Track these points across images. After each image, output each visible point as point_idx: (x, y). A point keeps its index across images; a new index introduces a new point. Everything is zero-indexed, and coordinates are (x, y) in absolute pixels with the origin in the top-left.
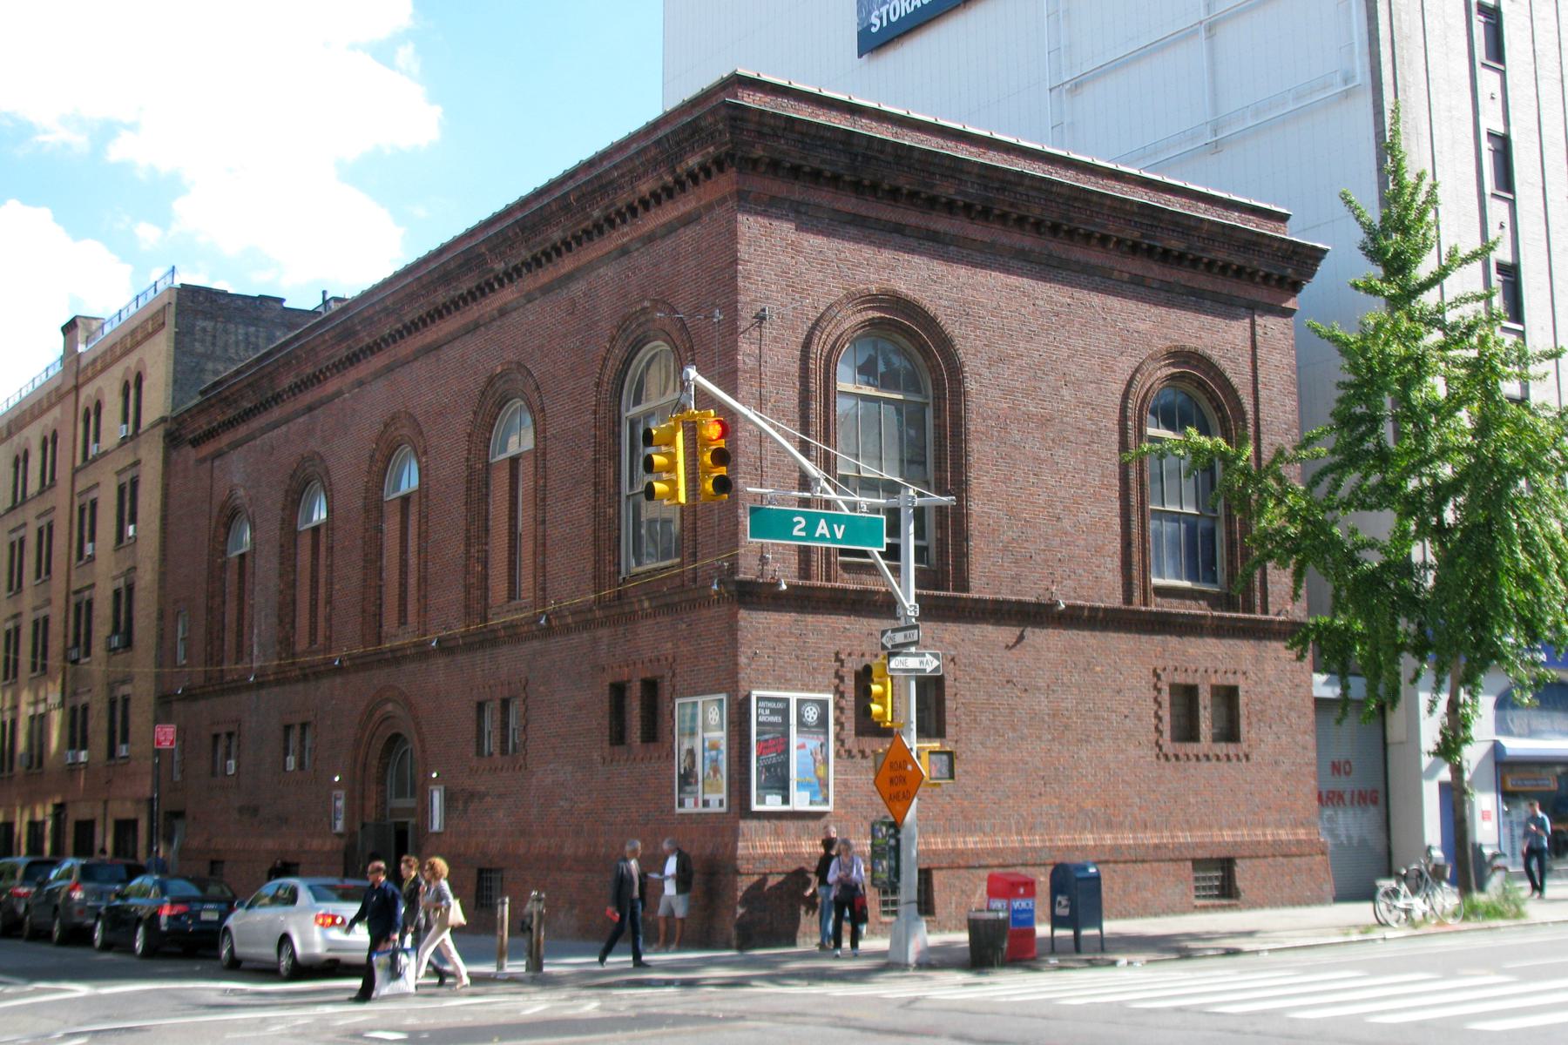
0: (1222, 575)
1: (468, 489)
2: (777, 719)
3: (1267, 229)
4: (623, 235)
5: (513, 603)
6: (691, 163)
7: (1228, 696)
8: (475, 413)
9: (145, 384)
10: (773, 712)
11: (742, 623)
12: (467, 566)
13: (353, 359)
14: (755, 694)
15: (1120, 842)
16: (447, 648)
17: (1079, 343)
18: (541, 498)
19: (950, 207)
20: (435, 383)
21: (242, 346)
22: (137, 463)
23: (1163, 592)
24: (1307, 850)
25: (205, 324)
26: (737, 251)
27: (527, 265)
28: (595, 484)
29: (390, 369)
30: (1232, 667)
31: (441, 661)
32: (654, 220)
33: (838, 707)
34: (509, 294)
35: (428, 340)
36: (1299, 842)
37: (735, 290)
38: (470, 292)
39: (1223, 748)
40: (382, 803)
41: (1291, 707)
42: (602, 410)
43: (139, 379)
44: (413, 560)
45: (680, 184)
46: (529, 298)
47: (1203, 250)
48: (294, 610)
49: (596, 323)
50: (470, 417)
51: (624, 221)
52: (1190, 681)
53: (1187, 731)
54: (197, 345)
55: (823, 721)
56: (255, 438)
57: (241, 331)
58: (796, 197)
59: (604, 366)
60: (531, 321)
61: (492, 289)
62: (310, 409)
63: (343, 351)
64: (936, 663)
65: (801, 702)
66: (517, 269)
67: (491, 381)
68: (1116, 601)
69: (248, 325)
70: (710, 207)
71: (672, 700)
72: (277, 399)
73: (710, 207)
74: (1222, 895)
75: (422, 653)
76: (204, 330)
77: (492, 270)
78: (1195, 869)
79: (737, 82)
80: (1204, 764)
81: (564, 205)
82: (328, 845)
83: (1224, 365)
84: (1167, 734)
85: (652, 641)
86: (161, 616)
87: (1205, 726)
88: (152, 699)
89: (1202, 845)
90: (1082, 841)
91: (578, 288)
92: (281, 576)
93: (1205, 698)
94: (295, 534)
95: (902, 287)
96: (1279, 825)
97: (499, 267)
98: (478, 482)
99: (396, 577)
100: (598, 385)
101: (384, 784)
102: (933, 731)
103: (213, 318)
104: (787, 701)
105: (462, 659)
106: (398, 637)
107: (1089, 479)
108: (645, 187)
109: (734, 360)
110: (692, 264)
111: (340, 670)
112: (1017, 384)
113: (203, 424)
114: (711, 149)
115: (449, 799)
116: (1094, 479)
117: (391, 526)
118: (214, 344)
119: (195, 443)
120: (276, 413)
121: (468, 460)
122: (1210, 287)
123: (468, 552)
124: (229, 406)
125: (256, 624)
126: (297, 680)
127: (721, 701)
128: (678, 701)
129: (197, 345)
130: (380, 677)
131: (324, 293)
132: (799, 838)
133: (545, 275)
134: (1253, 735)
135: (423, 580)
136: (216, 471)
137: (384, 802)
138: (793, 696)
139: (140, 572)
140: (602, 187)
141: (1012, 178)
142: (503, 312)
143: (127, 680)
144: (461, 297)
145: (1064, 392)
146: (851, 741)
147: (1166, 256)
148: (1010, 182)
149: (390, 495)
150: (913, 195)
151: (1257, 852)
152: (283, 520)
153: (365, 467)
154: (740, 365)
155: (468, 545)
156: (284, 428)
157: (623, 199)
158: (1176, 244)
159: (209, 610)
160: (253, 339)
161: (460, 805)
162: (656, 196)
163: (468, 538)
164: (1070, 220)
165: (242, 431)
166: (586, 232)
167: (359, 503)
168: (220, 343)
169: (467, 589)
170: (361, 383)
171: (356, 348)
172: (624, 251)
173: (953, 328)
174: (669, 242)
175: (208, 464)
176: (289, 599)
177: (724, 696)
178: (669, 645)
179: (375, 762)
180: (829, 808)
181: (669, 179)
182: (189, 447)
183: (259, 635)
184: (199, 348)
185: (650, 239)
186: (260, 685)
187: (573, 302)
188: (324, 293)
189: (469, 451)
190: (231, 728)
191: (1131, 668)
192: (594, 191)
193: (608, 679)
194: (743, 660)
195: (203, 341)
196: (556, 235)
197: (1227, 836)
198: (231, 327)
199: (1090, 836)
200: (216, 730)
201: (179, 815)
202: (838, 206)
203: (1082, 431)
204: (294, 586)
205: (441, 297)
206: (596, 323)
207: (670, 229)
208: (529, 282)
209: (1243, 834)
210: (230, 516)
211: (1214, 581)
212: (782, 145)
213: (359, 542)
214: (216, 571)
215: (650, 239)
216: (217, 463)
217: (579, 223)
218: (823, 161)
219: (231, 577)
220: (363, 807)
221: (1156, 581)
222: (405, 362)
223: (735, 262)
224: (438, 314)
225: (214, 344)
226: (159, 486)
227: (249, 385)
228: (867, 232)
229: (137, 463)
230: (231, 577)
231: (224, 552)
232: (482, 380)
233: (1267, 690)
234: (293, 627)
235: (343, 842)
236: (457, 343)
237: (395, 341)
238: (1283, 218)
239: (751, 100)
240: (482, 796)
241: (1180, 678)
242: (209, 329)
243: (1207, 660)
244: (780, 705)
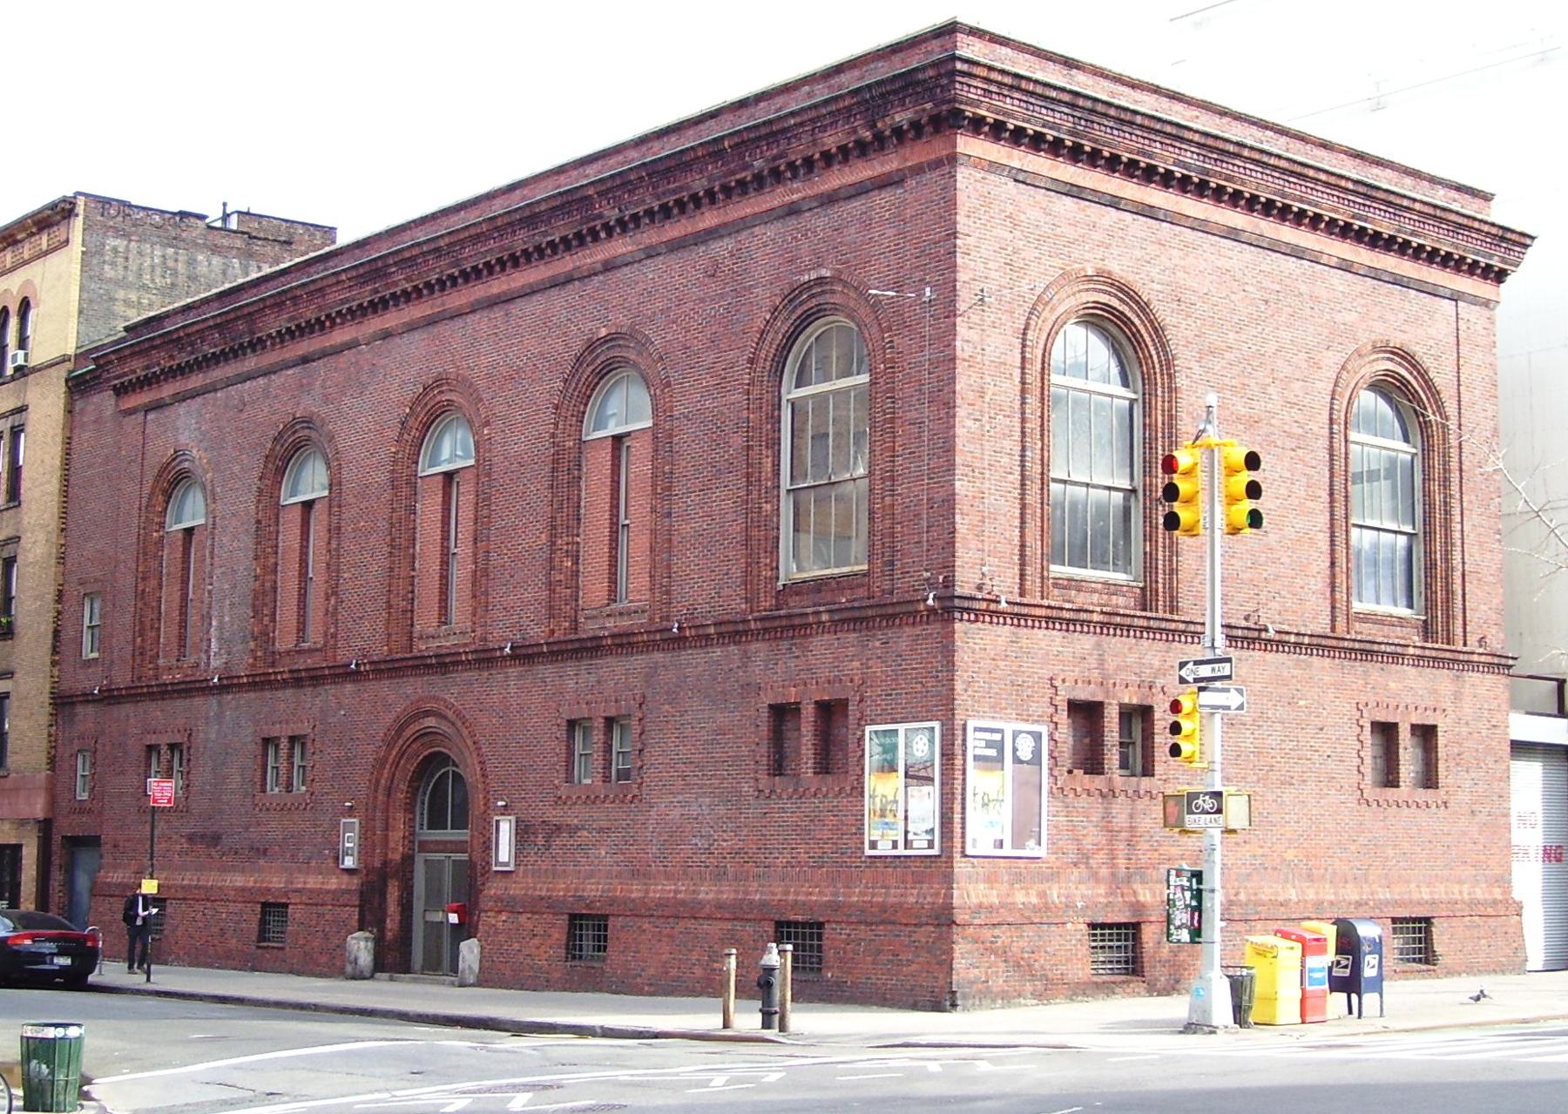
2: (992, 752)
3: (1470, 207)
4: (794, 192)
5: (613, 606)
6: (897, 118)
10: (989, 744)
11: (958, 643)
13: (378, 306)
14: (971, 724)
15: (1321, 896)
16: (525, 655)
17: (1285, 335)
18: (663, 486)
20: (510, 342)
21: (158, 271)
22: (22, 410)
23: (1365, 618)
25: (117, 242)
26: (955, 223)
27: (650, 213)
28: (748, 476)
29: (431, 321)
30: (1431, 704)
31: (514, 671)
32: (838, 178)
33: (1051, 738)
34: (620, 246)
35: (495, 290)
36: (1495, 902)
37: (953, 267)
38: (564, 239)
39: (1423, 795)
41: (1489, 750)
42: (756, 392)
44: (462, 549)
45: (879, 138)
46: (651, 253)
47: (1413, 234)
51: (795, 177)
53: (1389, 778)
54: (107, 267)
55: (1036, 759)
56: (216, 390)
58: (1016, 164)
60: (649, 286)
61: (596, 238)
62: (305, 360)
63: (365, 295)
65: (1016, 735)
66: (635, 218)
67: (591, 346)
68: (1321, 625)
70: (918, 170)
71: (861, 727)
72: (257, 345)
73: (918, 170)
74: (1127, 972)
76: (115, 250)
77: (600, 216)
82: (333, 883)
83: (1427, 362)
84: (1369, 779)
85: (826, 662)
87: (1112, 758)
88: (46, 698)
90: (1417, 895)
91: (721, 248)
93: (1405, 736)
97: (612, 214)
98: (565, 465)
100: (751, 361)
101: (413, 812)
102: (1139, 769)
103: (126, 236)
104: (1001, 731)
105: (546, 671)
106: (431, 635)
107: (1295, 488)
108: (831, 140)
109: (950, 345)
110: (890, 232)
112: (1227, 381)
114: (928, 106)
115: (523, 833)
116: (1300, 491)
119: (121, 391)
120: (251, 362)
121: (553, 436)
124: (181, 350)
126: (284, 684)
127: (933, 729)
128: (868, 729)
129: (107, 267)
130: (412, 689)
131: (225, 205)
133: (675, 229)
134: (1450, 780)
136: (150, 428)
137: (413, 834)
138: (1009, 728)
139: (25, 542)
140: (773, 134)
142: (609, 267)
144: (551, 244)
145: (1271, 390)
146: (1063, 778)
147: (1375, 241)
149: (425, 469)
150: (1133, 164)
152: (260, 491)
153: (394, 434)
154: (959, 353)
155: (553, 538)
156: (261, 381)
157: (797, 151)
158: (1386, 228)
159: (140, 595)
160: (171, 264)
161: (540, 840)
162: (844, 150)
163: (554, 527)
164: (1284, 195)
165: (196, 381)
166: (742, 184)
167: (382, 477)
169: (551, 586)
170: (387, 335)
171: (387, 293)
172: (793, 210)
173: (1164, 313)
174: (856, 204)
175: (140, 417)
177: (936, 725)
178: (856, 664)
179: (403, 787)
181: (867, 135)
183: (221, 628)
184: (109, 271)
185: (830, 199)
186: (222, 689)
187: (716, 265)
188: (225, 205)
190: (177, 739)
191: (1340, 699)
192: (759, 138)
193: (767, 699)
194: (959, 686)
195: (113, 264)
196: (699, 184)
198: (147, 247)
200: (152, 740)
201: (93, 842)
203: (1289, 435)
205: (520, 240)
207: (860, 190)
208: (651, 236)
209: (1440, 892)
210: (174, 480)
213: (383, 524)
214: (148, 549)
215: (830, 199)
216: (151, 416)
217: (733, 173)
221: (1357, 606)
222: (458, 314)
223: (954, 235)
224: (515, 261)
226: (59, 439)
227: (217, 326)
229: (22, 410)
230: (170, 556)
231: (162, 525)
232: (578, 346)
233: (1465, 730)
234: (274, 620)
235: (355, 882)
236: (538, 297)
237: (443, 289)
238: (1486, 197)
240: (573, 830)
243: (1410, 692)
244: (997, 737)
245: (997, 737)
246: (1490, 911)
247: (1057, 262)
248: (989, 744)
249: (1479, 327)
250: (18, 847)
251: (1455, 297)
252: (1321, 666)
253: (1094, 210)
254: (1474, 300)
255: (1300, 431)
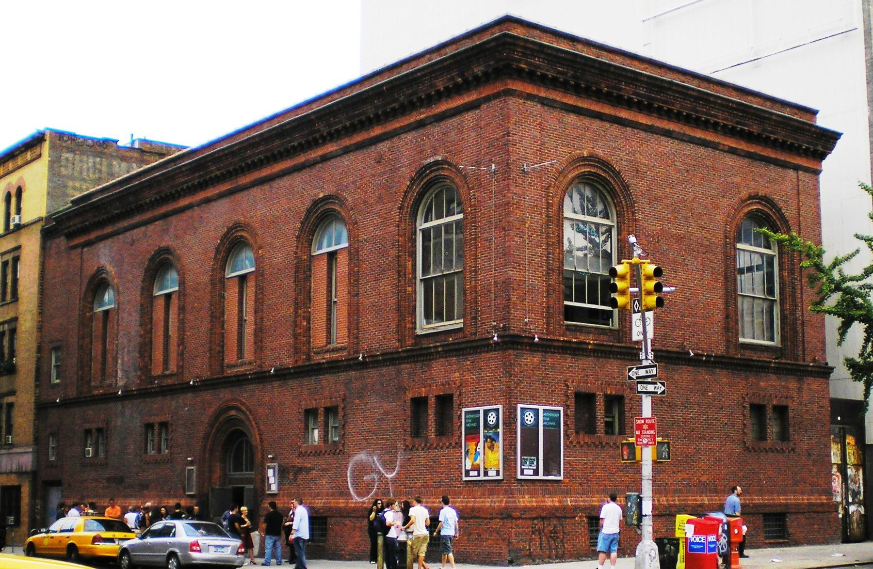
0: (777, 337)
1: (296, 272)
2: (553, 424)
7: (782, 411)
8: (302, 223)
9: (24, 195)
12: (295, 322)
16: (283, 375)
18: (354, 278)
19: (629, 104)
21: (91, 171)
24: (827, 509)
28: (399, 272)
33: (566, 415)
36: (823, 504)
40: (224, 475)
43: (19, 192)
47: (772, 133)
48: (151, 348)
49: (398, 169)
50: (299, 225)
52: (761, 402)
57: (91, 160)
59: (405, 196)
64: (663, 388)
65: (486, 412)
69: (95, 156)
71: (460, 409)
75: (261, 377)
76: (67, 159)
78: (765, 520)
79: (508, 20)
80: (770, 454)
81: (378, 92)
86: (39, 349)
89: (766, 505)
92: (141, 325)
94: (152, 298)
95: (600, 153)
96: (811, 493)
99: (235, 327)
103: (72, 151)
110: (473, 134)
111: (194, 389)
113: (76, 223)
114: (492, 63)
117: (232, 294)
118: (73, 169)
122: (773, 156)
123: (296, 312)
125: (120, 356)
130: (225, 395)
132: (544, 497)
135: (259, 332)
139: (21, 321)
141: (666, 85)
143: (13, 393)
148: (664, 88)
151: (798, 510)
152: (143, 288)
158: (755, 129)
159: (81, 347)
160: (98, 166)
163: (297, 304)
164: (697, 112)
168: (77, 168)
169: (296, 336)
175: (79, 250)
176: (147, 340)
178: (457, 374)
180: (561, 478)
182: (63, 238)
183: (122, 364)
184: (64, 171)
189: (297, 247)
197: (782, 499)
198: (85, 158)
199: (706, 498)
200: (87, 426)
202: (565, 100)
204: (150, 332)
206: (398, 169)
209: (791, 499)
210: (98, 284)
211: (772, 339)
212: (537, 61)
213: (207, 305)
214: (86, 321)
216: (85, 249)
218: (559, 72)
219: (97, 326)
220: (210, 478)
221: (741, 340)
225: (73, 169)
226: (37, 264)
228: (581, 117)
230: (97, 326)
231: (92, 309)
232: (308, 204)
234: (151, 359)
238: (814, 113)
239: (518, 32)
240: (308, 470)
241: (756, 401)
242: (70, 159)
244: (557, 415)
245: (557, 415)
246: (820, 509)
247: (566, 150)
248: (552, 419)
249: (810, 185)
250: (18, 488)
251: (797, 168)
252: (723, 377)
253: (587, 121)
254: (807, 170)
255: (708, 243)
